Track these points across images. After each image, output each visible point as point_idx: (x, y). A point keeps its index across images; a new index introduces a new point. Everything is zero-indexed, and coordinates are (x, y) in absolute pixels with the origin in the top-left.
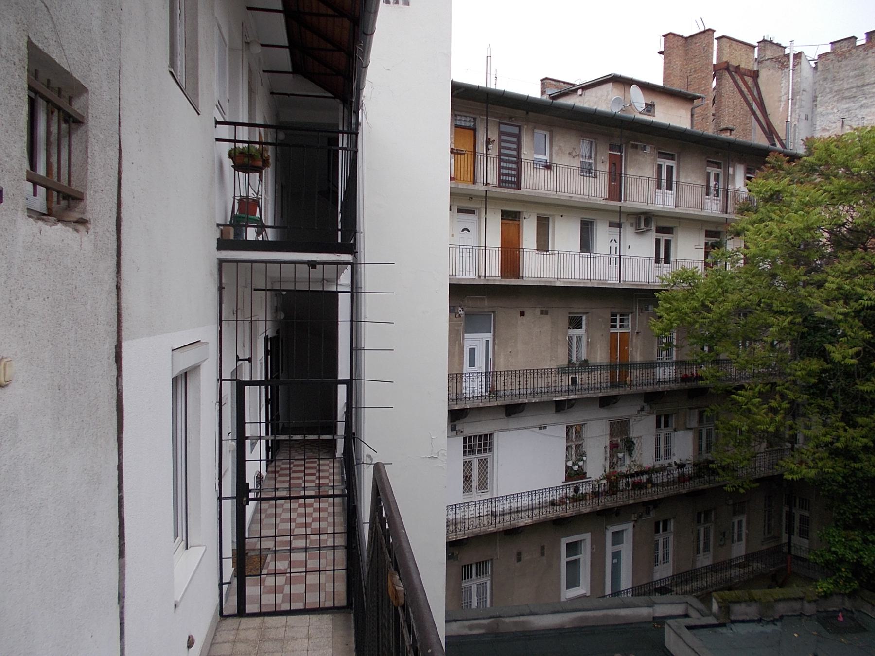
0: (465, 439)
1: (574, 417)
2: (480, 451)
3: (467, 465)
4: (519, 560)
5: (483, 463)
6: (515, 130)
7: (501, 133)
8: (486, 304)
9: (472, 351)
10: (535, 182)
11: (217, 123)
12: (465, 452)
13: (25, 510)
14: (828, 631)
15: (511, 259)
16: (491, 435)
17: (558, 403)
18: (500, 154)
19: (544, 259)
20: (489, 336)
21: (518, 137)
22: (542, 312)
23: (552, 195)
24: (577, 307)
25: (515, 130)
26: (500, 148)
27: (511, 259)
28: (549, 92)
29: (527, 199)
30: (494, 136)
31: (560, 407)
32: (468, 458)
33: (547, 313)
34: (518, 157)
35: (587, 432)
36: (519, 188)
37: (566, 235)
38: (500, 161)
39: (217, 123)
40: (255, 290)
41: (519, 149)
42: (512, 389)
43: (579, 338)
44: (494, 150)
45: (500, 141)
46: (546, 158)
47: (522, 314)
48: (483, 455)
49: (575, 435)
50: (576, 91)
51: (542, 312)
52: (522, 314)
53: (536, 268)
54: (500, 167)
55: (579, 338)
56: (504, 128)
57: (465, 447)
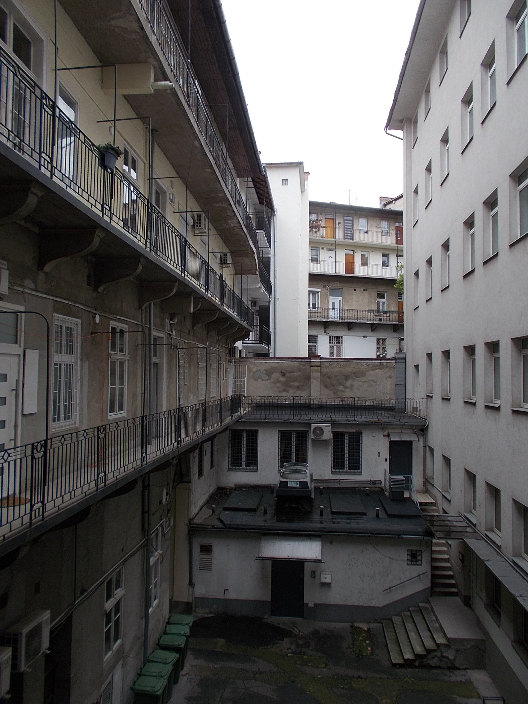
0: (330, 337)
1: (381, 335)
2: (337, 343)
3: (332, 348)
5: (339, 348)
6: (351, 219)
7: (344, 220)
8: (338, 285)
9: (333, 303)
10: (359, 237)
11: (174, 212)
12: (330, 343)
15: (350, 266)
16: (342, 337)
18: (344, 228)
19: (364, 268)
20: (341, 298)
21: (352, 221)
22: (364, 290)
23: (364, 242)
24: (382, 289)
25: (351, 219)
26: (344, 225)
27: (350, 266)
28: (383, 203)
29: (376, 246)
30: (342, 222)
31: (373, 328)
32: (332, 345)
33: (366, 290)
34: (353, 229)
35: (388, 342)
36: (353, 240)
37: (375, 259)
38: (344, 231)
39: (174, 212)
40: (58, 70)
41: (353, 226)
42: (350, 317)
43: (383, 303)
44: (342, 226)
45: (344, 223)
46: (366, 229)
47: (355, 290)
48: (338, 345)
49: (381, 342)
50: (392, 202)
51: (364, 290)
52: (355, 290)
53: (360, 271)
54: (344, 233)
55: (383, 303)
56: (345, 218)
57: (330, 340)
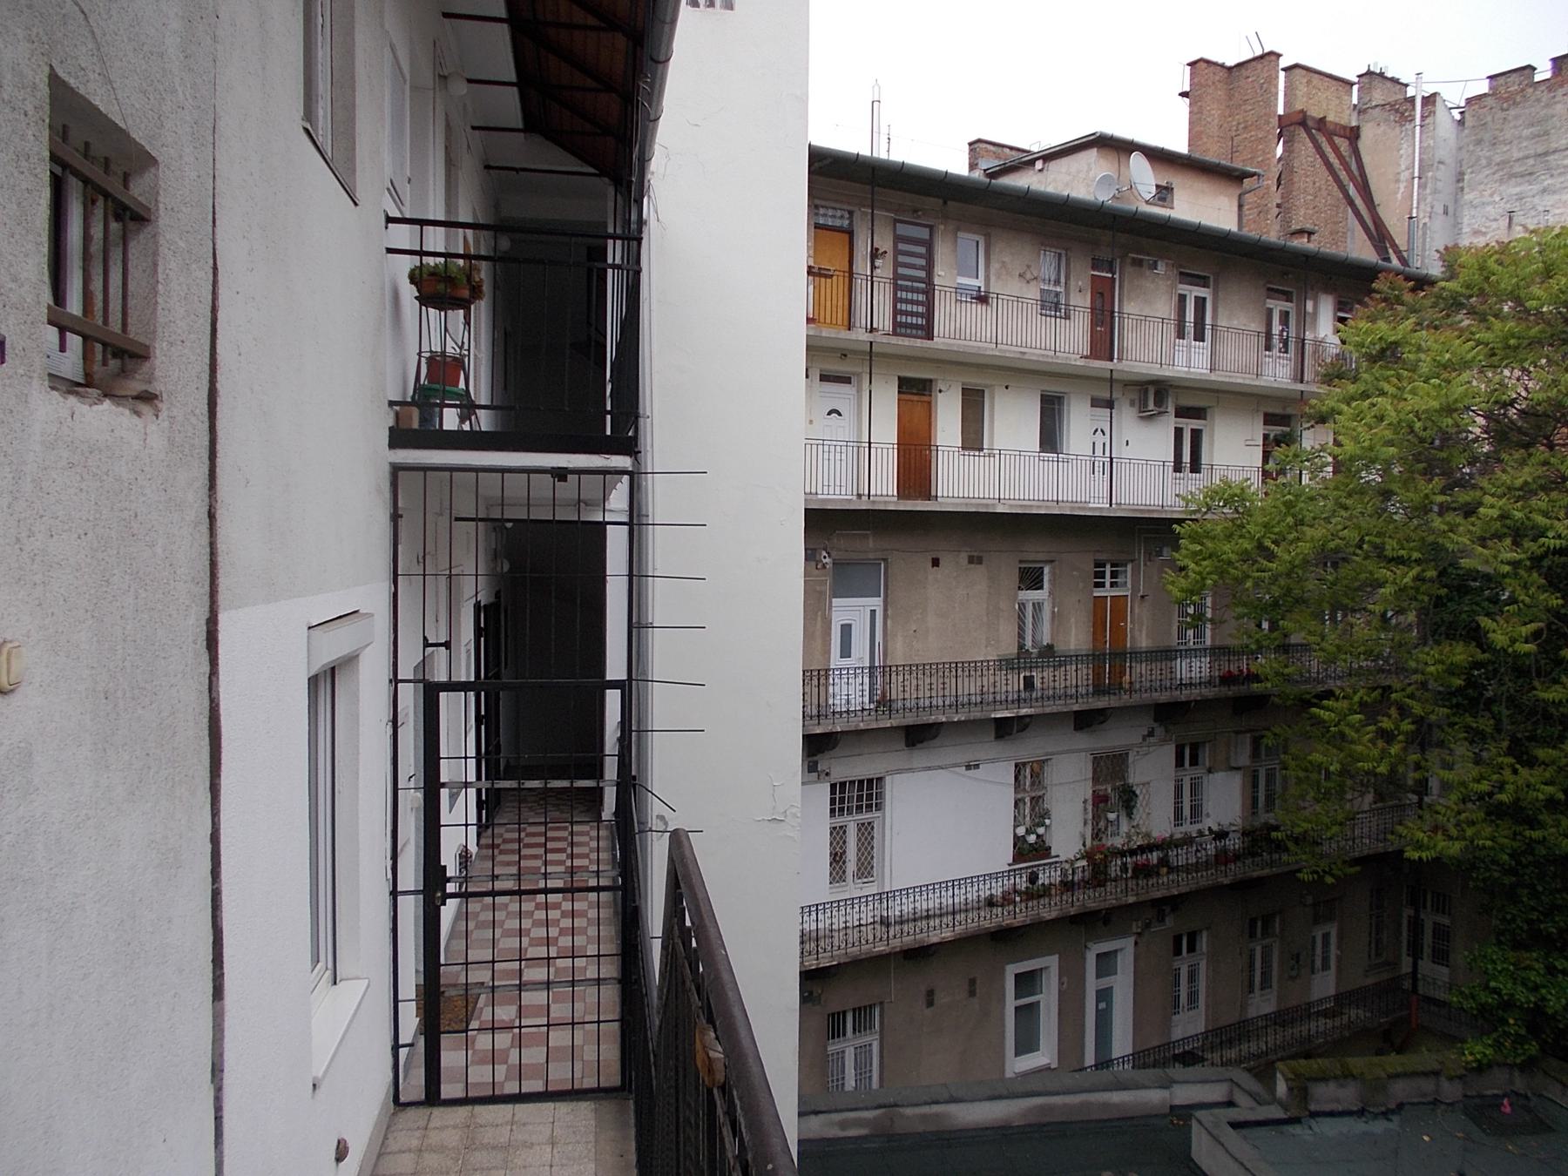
0: (833, 786)
1: (1029, 748)
2: (859, 808)
3: (838, 834)
5: (866, 830)
6: (923, 233)
7: (898, 239)
8: (870, 545)
9: (846, 630)
10: (959, 325)
12: (832, 811)
15: (915, 465)
16: (880, 779)
18: (896, 277)
19: (975, 464)
20: (876, 603)
21: (929, 245)
22: (971, 560)
23: (990, 349)
24: (1034, 551)
25: (923, 233)
26: (896, 265)
27: (915, 465)
28: (983, 165)
30: (885, 243)
31: (1004, 729)
32: (839, 821)
33: (979, 561)
34: (929, 281)
35: (1052, 775)
36: (930, 336)
37: (1014, 421)
38: (896, 288)
41: (929, 268)
42: (918, 698)
43: (1038, 607)
44: (885, 269)
45: (897, 252)
46: (979, 282)
47: (936, 563)
48: (865, 816)
49: (1030, 779)
50: (1032, 163)
51: (971, 560)
52: (936, 563)
53: (960, 481)
54: (896, 300)
55: (1038, 607)
56: (903, 230)
57: (833, 801)
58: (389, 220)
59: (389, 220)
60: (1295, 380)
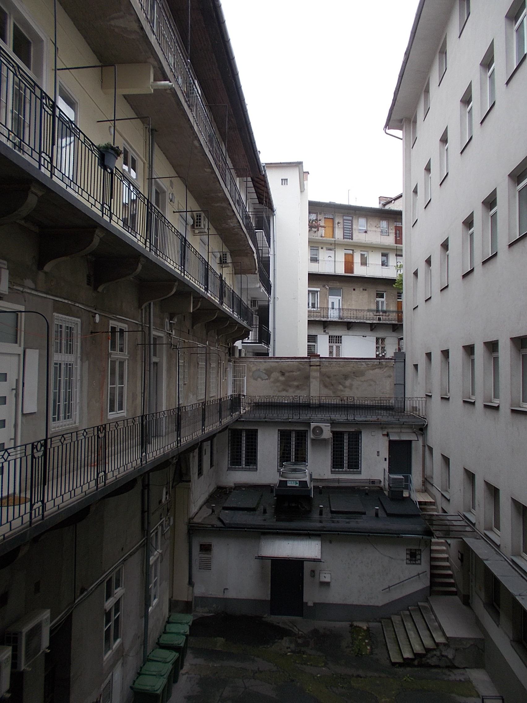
0: (330, 337)
1: (381, 334)
2: (336, 342)
3: (331, 347)
4: (378, 455)
5: (338, 348)
6: (351, 218)
7: (344, 220)
8: (338, 285)
9: (333, 303)
10: (359, 237)
12: (329, 342)
13: (85, 434)
14: (175, 90)
15: (349, 266)
16: (341, 337)
17: (371, 324)
18: (344, 228)
19: (364, 268)
20: (340, 298)
21: (352, 221)
22: (363, 290)
23: (363, 242)
24: (381, 289)
25: (351, 218)
26: (344, 225)
27: (349, 266)
28: (382, 202)
30: (341, 221)
31: (373, 327)
32: (331, 344)
33: (366, 290)
34: (352, 229)
35: (387, 341)
36: (352, 239)
37: (375, 259)
38: (344, 230)
41: (352, 226)
42: (349, 317)
43: (382, 302)
44: (341, 226)
45: (344, 223)
46: (365, 229)
47: (354, 290)
48: (337, 344)
49: (380, 341)
50: (391, 201)
51: (363, 290)
52: (354, 290)
53: (359, 271)
54: (344, 233)
55: (382, 302)
56: (345, 218)
57: (329, 340)
58: (174, 212)
59: (174, 212)
60: (396, 243)
